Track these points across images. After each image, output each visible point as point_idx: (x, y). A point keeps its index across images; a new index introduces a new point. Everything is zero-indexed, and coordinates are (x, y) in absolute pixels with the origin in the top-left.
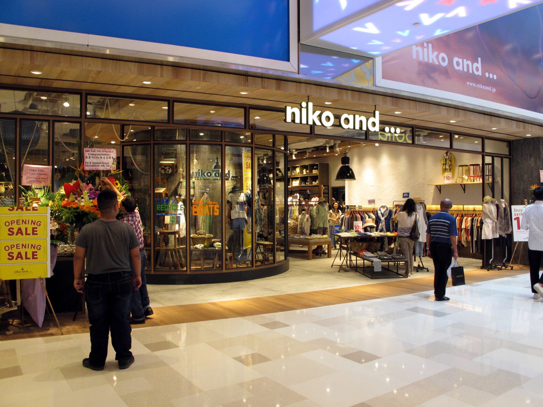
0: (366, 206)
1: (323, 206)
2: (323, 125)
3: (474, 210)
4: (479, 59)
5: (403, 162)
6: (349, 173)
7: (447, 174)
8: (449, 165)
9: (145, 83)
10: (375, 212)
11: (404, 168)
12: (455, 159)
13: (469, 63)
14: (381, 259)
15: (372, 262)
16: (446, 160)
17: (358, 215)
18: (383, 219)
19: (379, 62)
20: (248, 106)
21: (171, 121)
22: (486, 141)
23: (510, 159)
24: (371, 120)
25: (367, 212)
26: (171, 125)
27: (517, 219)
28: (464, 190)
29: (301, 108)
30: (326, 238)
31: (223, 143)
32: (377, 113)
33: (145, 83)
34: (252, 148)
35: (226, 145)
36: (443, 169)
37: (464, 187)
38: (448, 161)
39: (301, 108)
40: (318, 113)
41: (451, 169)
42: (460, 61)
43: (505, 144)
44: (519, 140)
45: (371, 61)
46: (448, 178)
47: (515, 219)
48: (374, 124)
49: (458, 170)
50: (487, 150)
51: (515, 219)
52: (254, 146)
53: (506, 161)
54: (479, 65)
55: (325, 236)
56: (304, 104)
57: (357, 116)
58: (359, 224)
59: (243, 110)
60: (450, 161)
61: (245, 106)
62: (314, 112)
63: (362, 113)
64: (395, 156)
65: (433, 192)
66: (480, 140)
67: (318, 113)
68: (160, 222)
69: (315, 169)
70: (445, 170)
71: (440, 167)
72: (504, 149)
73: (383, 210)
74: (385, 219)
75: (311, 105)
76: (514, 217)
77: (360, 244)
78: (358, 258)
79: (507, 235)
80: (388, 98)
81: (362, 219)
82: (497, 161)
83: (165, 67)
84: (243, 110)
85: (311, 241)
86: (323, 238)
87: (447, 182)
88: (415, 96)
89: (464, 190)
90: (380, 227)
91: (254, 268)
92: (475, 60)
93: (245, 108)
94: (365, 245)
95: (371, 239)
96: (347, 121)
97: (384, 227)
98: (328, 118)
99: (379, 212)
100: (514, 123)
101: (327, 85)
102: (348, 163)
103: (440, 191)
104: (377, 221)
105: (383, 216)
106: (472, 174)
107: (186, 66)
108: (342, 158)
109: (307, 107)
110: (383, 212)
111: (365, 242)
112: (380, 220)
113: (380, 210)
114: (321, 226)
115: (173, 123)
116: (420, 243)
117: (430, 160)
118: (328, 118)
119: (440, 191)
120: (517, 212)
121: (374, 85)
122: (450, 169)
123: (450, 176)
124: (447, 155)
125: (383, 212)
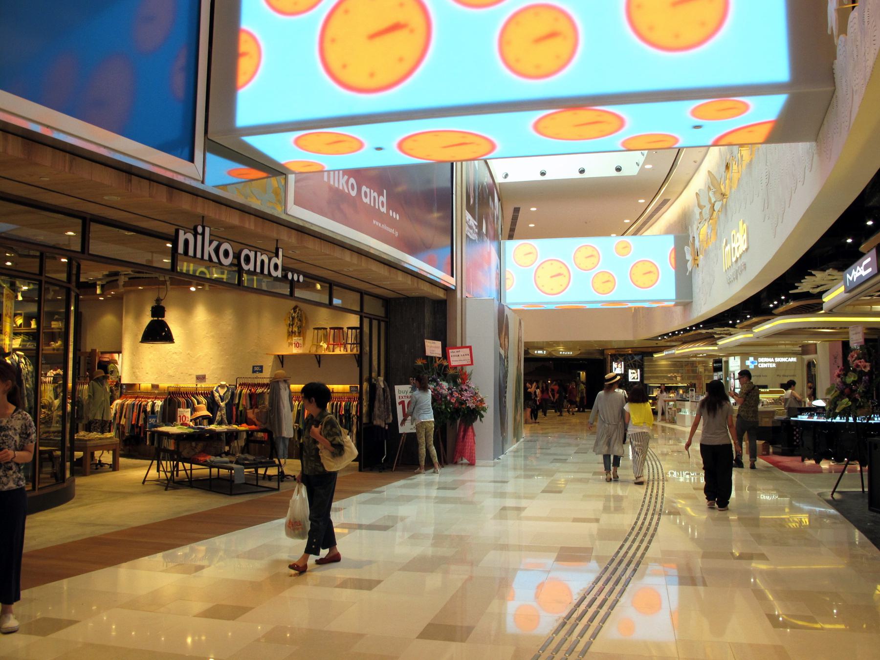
0: (189, 384)
1: (103, 384)
5: (229, 318)
6: (165, 331)
7: (295, 339)
8: (298, 325)
10: (209, 396)
11: (230, 328)
12: (306, 318)
13: (376, 194)
14: (243, 464)
15: (231, 469)
16: (293, 318)
17: (182, 400)
18: (222, 404)
19: (291, 178)
20: (88, 217)
22: (366, 297)
23: (386, 323)
24: (274, 260)
25: (195, 393)
27: (402, 403)
30: (110, 438)
34: (40, 282)
36: (289, 332)
37: (319, 358)
38: (296, 320)
39: (195, 234)
40: (215, 244)
41: (301, 333)
42: (368, 190)
43: (380, 303)
44: (399, 299)
45: (281, 179)
46: (297, 345)
47: (400, 403)
48: (276, 267)
49: (310, 334)
50: (366, 310)
51: (400, 403)
52: (43, 279)
53: (383, 324)
54: (383, 199)
55: (108, 435)
56: (200, 229)
57: (259, 254)
58: (185, 413)
59: (80, 221)
60: (300, 320)
62: (211, 242)
63: (264, 251)
64: (215, 309)
65: (271, 364)
66: (358, 296)
68: (553, 408)
69: (57, 320)
70: (291, 334)
71: (284, 329)
72: (374, 308)
73: (222, 392)
74: (226, 404)
76: (398, 401)
77: (194, 444)
78: (194, 466)
79: (389, 425)
80: (294, 231)
81: (189, 405)
82: (375, 323)
83: (10, 136)
84: (80, 221)
85: (90, 444)
86: (107, 438)
87: (295, 351)
90: (218, 418)
91: (36, 493)
92: (380, 194)
94: (201, 445)
95: (215, 435)
96: (247, 259)
97: (225, 417)
98: (226, 254)
99: (217, 395)
100: (410, 277)
102: (163, 316)
103: (282, 363)
104: (212, 406)
105: (222, 399)
106: (331, 342)
108: (153, 308)
109: (203, 234)
110: (222, 394)
111: (199, 443)
112: (219, 406)
113: (217, 391)
114: (99, 418)
116: (284, 438)
117: (267, 320)
118: (226, 254)
120: (402, 395)
122: (299, 333)
123: (301, 342)
124: (295, 312)
125: (222, 394)
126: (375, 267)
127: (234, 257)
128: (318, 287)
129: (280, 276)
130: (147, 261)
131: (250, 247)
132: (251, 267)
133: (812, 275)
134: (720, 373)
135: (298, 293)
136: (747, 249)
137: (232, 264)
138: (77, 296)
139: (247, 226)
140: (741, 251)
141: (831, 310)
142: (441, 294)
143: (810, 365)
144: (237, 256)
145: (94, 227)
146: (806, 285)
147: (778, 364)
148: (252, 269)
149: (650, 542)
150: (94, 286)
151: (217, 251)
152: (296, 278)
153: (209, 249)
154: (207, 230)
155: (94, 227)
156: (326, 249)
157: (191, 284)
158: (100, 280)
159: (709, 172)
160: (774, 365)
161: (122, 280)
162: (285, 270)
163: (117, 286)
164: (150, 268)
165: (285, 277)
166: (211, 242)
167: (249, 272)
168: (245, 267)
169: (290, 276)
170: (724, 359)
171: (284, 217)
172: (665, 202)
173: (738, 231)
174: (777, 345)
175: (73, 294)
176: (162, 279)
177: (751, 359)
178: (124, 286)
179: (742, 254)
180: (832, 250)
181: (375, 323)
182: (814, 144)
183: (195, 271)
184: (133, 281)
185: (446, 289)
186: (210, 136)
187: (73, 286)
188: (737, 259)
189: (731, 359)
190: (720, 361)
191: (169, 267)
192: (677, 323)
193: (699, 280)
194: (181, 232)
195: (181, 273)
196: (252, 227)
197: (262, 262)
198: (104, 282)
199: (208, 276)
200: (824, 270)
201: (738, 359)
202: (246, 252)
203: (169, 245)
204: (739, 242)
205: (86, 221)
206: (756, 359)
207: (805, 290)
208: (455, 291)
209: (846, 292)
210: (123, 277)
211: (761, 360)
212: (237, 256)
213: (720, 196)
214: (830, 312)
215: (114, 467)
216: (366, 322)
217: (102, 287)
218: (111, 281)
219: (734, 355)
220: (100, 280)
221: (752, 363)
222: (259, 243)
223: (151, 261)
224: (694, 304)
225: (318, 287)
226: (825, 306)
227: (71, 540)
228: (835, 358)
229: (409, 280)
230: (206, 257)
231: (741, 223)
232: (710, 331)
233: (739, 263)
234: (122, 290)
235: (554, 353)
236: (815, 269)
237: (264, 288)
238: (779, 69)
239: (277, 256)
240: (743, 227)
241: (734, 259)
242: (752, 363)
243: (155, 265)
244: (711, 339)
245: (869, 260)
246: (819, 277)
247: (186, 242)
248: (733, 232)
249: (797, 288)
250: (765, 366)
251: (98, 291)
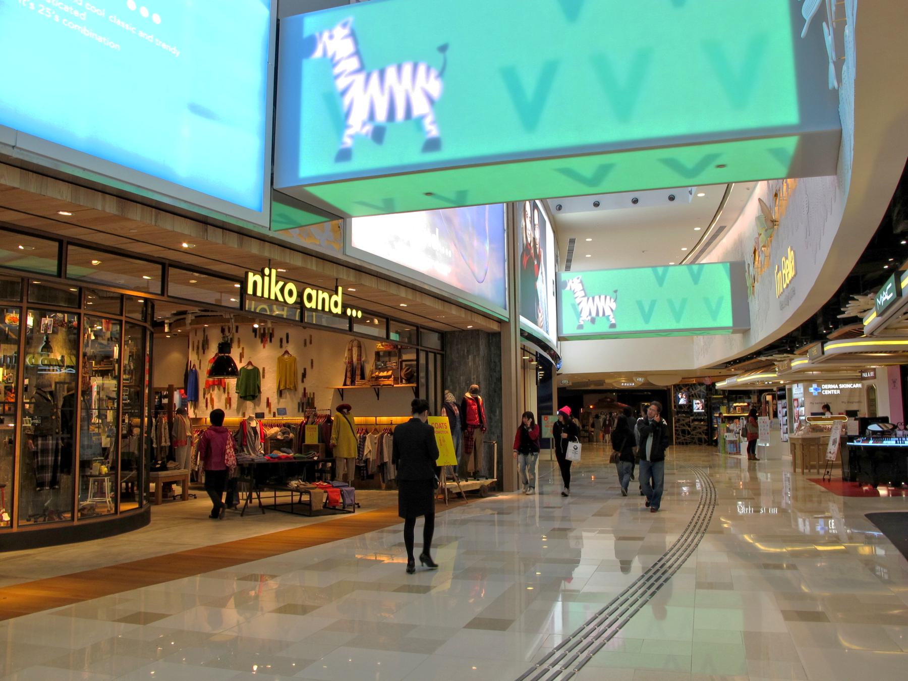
2: (285, 302)
3: (391, 424)
4: (437, 230)
9: (61, 213)
20: (167, 262)
21: (63, 274)
23: (442, 356)
24: (334, 298)
26: (62, 280)
28: (378, 395)
29: (263, 275)
31: (82, 311)
32: (340, 289)
33: (61, 213)
35: (28, 308)
39: (263, 275)
40: (281, 284)
45: (341, 221)
47: (79, 511)
48: (336, 304)
52: (123, 319)
53: (439, 357)
56: (267, 271)
57: (320, 292)
59: (57, 244)
61: (164, 261)
62: (277, 282)
63: (324, 289)
67: (281, 284)
75: (274, 271)
82: (431, 356)
83: (107, 196)
84: (57, 244)
88: (27, 159)
89: (378, 395)
93: (61, 242)
96: (310, 298)
98: (291, 293)
101: (176, 211)
103: (342, 396)
107: (132, 198)
109: (270, 276)
115: (66, 278)
118: (291, 293)
119: (342, 396)
121: (344, 254)
126: (429, 302)
127: (298, 296)
128: (376, 321)
129: (340, 312)
130: (216, 300)
131: (313, 286)
132: (313, 305)
133: (853, 299)
134: (784, 401)
135: (357, 328)
136: (795, 275)
137: (296, 303)
138: (152, 334)
139: (309, 267)
140: (790, 277)
141: (872, 334)
142: (495, 327)
143: (871, 390)
144: (300, 295)
145: (172, 271)
146: (850, 310)
147: (841, 390)
148: (314, 307)
149: (688, 556)
150: (162, 324)
151: (282, 290)
152: (354, 315)
153: (275, 290)
154: (274, 271)
155: (172, 271)
156: (383, 286)
157: (254, 321)
158: (167, 318)
159: (760, 200)
160: (839, 392)
161: (190, 318)
162: (345, 307)
163: (185, 325)
164: (218, 306)
165: (344, 312)
166: (277, 282)
167: (311, 309)
168: (308, 305)
169: (349, 312)
170: (787, 387)
171: (340, 256)
172: (721, 229)
173: (787, 258)
174: (839, 370)
175: (148, 333)
176: (228, 316)
177: (815, 386)
178: (191, 324)
179: (793, 281)
180: (864, 278)
181: (431, 356)
182: (835, 177)
183: (255, 309)
184: (199, 319)
185: (500, 321)
186: (275, 187)
187: (148, 325)
188: (788, 285)
189: (795, 387)
190: (783, 389)
191: (238, 305)
192: (736, 349)
193: (755, 305)
194: (251, 274)
195: (250, 311)
196: (314, 268)
197: (324, 300)
198: (172, 321)
199: (268, 313)
200: (866, 295)
201: (801, 386)
202: (308, 291)
203: (238, 286)
204: (789, 270)
205: (165, 266)
206: (819, 385)
207: (853, 314)
208: (508, 323)
209: (878, 316)
210: (190, 316)
211: (825, 386)
212: (300, 295)
213: (770, 224)
214: (872, 336)
215: (183, 497)
216: (422, 356)
217: (170, 325)
218: (179, 318)
219: (797, 382)
220: (167, 318)
221: (816, 389)
222: (320, 282)
223: (220, 300)
224: (752, 331)
225: (376, 321)
226: (865, 330)
227: (154, 556)
228: (894, 382)
229: (463, 314)
230: (273, 297)
231: (789, 249)
232: (769, 358)
233: (790, 288)
234: (188, 327)
235: (615, 385)
236: (858, 293)
237: (324, 324)
238: (787, 112)
239: (337, 293)
240: (791, 254)
241: (785, 286)
242: (816, 389)
243: (224, 304)
244: (768, 367)
245: (890, 285)
246: (861, 301)
247: (255, 283)
248: (783, 259)
249: (844, 312)
250: (830, 392)
251: (167, 330)
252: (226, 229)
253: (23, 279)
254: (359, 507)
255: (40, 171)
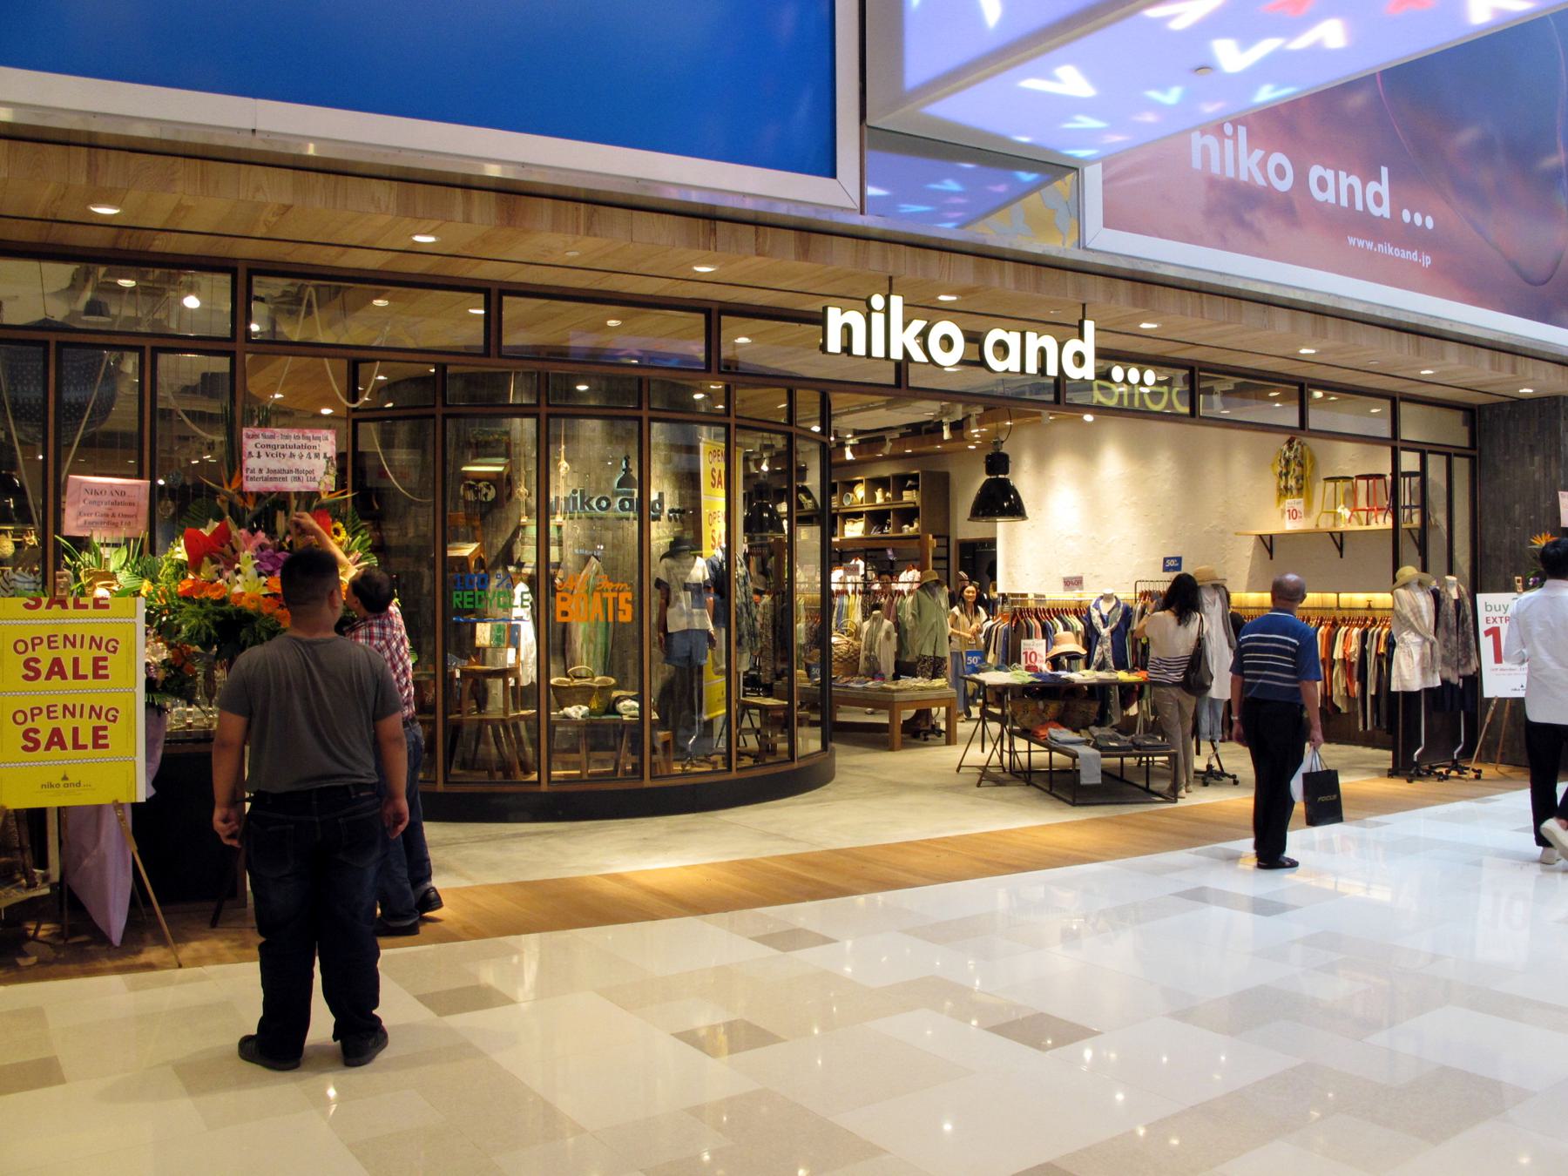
0: (1057, 595)
1: (934, 595)
2: (931, 361)
3: (1369, 608)
4: (1384, 171)
5: (1164, 468)
6: (1009, 500)
7: (1291, 502)
8: (1297, 476)
9: (418, 238)
10: (1082, 612)
11: (1167, 487)
12: (1313, 459)
13: (1355, 181)
14: (1101, 749)
15: (1075, 756)
16: (1288, 461)
17: (1034, 623)
18: (1105, 632)
19: (1093, 178)
20: (715, 307)
21: (493, 351)
22: (1405, 408)
23: (1472, 459)
24: (1073, 346)
25: (1059, 612)
26: (494, 361)
27: (1494, 632)
28: (1341, 549)
29: (868, 313)
30: (940, 688)
31: (645, 413)
32: (1089, 326)
33: (418, 238)
34: (728, 427)
35: (652, 419)
36: (1279, 489)
37: (1339, 541)
38: (1293, 465)
39: (868, 313)
40: (918, 325)
41: (1302, 488)
42: (1329, 175)
43: (1457, 417)
44: (1500, 404)
45: (1070, 177)
46: (1294, 514)
47: (1487, 633)
48: (1080, 359)
49: (1322, 491)
50: (1407, 434)
51: (1487, 633)
52: (732, 421)
53: (1462, 466)
54: (1384, 188)
55: (938, 682)
56: (877, 301)
57: (1031, 336)
58: (1035, 647)
59: (701, 317)
60: (1301, 465)
61: (708, 305)
62: (906, 325)
63: (1044, 325)
64: (1140, 452)
65: (1249, 553)
66: (1387, 404)
67: (918, 325)
69: (910, 488)
70: (1284, 492)
71: (1270, 483)
72: (1455, 432)
73: (1105, 608)
74: (1112, 632)
75: (897, 302)
76: (1483, 627)
77: (1041, 705)
78: (1034, 747)
79: (1465, 678)
80: (1122, 284)
81: (1047, 632)
84: (701, 317)
85: (898, 697)
86: (933, 689)
87: (1290, 526)
89: (1341, 549)
90: (1097, 657)
91: (734, 775)
92: (1371, 175)
93: (708, 313)
94: (1053, 707)
95: (1072, 689)
96: (1002, 348)
97: (1109, 656)
98: (947, 342)
99: (1095, 614)
100: (1485, 354)
101: (945, 245)
102: (1006, 472)
103: (1271, 551)
104: (1090, 637)
105: (1105, 623)
106: (1362, 503)
107: (538, 191)
108: (988, 457)
109: (887, 311)
110: (1105, 613)
111: (1053, 700)
112: (1099, 635)
113: (1097, 606)
114: (928, 652)
115: (500, 356)
116: (1213, 701)
117: (1240, 463)
118: (947, 342)
119: (1271, 551)
120: (1494, 614)
121: (1081, 244)
122: (1300, 490)
123: (1300, 508)
124: (1290, 448)
125: (1105, 613)
252: (68, 144)
253: (640, 380)
254: (1236, 783)
255: (166, 149)
